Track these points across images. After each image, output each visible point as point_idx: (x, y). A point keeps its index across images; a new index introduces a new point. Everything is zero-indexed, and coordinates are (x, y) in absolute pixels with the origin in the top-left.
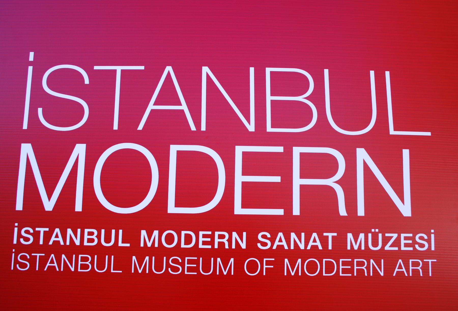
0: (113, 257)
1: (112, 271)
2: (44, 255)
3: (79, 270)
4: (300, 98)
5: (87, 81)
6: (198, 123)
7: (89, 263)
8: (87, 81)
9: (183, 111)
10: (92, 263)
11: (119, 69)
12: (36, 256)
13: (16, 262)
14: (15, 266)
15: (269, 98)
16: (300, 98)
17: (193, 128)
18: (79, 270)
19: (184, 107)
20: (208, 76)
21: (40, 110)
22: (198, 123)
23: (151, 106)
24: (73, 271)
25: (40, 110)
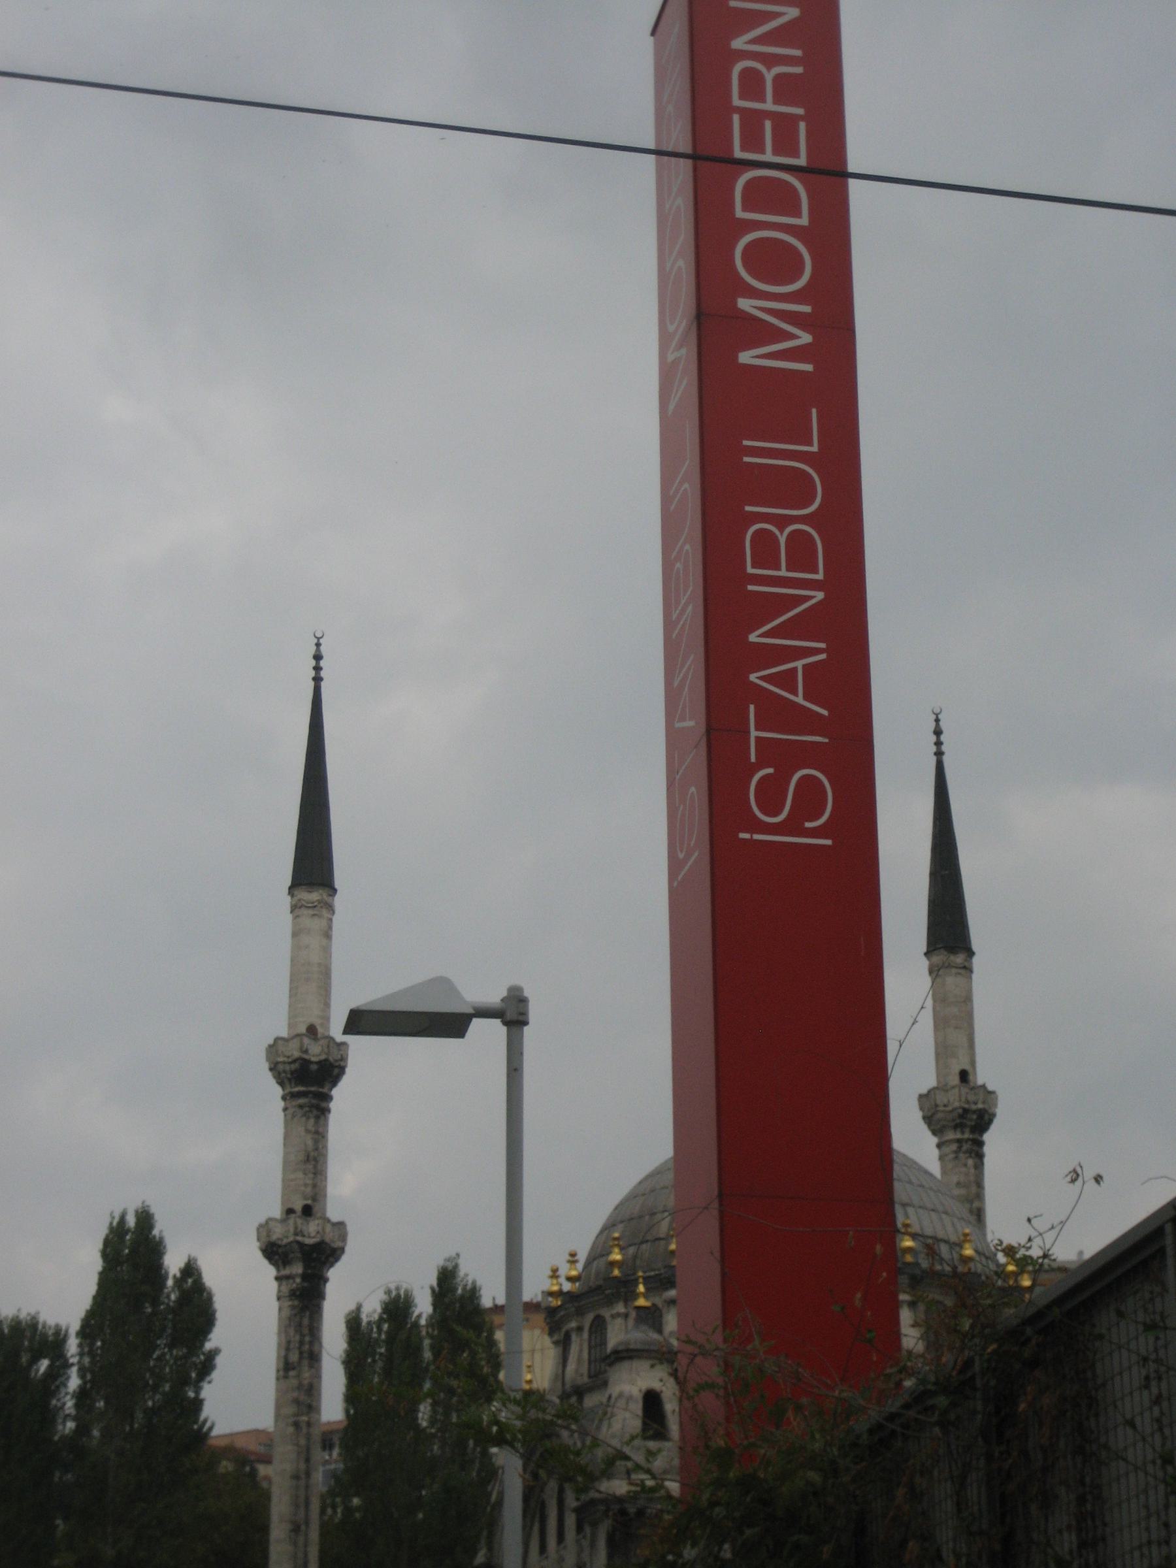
0: (746, 443)
1: (815, 448)
2: (752, 708)
3: (820, 576)
4: (782, 540)
5: (770, 770)
6: (818, 651)
7: (782, 532)
8: (770, 770)
9: (804, 666)
10: (782, 522)
11: (754, 733)
12: (758, 739)
13: (792, 826)
14: (813, 833)
15: (783, 573)
16: (782, 540)
17: (823, 656)
18: (820, 576)
19: (799, 664)
20: (760, 636)
21: (808, 825)
22: (818, 651)
23: (800, 699)
24: (825, 594)
25: (808, 825)
